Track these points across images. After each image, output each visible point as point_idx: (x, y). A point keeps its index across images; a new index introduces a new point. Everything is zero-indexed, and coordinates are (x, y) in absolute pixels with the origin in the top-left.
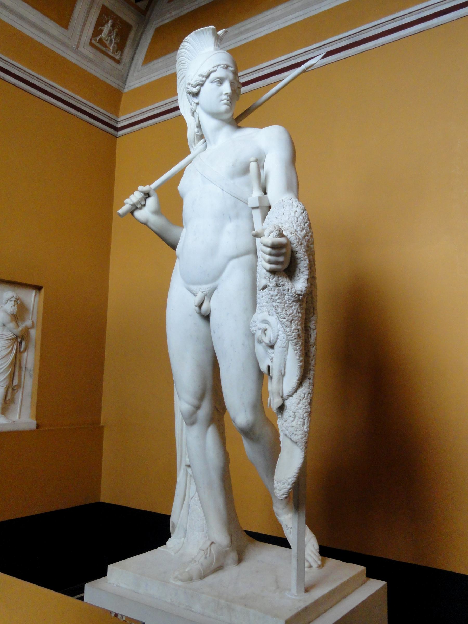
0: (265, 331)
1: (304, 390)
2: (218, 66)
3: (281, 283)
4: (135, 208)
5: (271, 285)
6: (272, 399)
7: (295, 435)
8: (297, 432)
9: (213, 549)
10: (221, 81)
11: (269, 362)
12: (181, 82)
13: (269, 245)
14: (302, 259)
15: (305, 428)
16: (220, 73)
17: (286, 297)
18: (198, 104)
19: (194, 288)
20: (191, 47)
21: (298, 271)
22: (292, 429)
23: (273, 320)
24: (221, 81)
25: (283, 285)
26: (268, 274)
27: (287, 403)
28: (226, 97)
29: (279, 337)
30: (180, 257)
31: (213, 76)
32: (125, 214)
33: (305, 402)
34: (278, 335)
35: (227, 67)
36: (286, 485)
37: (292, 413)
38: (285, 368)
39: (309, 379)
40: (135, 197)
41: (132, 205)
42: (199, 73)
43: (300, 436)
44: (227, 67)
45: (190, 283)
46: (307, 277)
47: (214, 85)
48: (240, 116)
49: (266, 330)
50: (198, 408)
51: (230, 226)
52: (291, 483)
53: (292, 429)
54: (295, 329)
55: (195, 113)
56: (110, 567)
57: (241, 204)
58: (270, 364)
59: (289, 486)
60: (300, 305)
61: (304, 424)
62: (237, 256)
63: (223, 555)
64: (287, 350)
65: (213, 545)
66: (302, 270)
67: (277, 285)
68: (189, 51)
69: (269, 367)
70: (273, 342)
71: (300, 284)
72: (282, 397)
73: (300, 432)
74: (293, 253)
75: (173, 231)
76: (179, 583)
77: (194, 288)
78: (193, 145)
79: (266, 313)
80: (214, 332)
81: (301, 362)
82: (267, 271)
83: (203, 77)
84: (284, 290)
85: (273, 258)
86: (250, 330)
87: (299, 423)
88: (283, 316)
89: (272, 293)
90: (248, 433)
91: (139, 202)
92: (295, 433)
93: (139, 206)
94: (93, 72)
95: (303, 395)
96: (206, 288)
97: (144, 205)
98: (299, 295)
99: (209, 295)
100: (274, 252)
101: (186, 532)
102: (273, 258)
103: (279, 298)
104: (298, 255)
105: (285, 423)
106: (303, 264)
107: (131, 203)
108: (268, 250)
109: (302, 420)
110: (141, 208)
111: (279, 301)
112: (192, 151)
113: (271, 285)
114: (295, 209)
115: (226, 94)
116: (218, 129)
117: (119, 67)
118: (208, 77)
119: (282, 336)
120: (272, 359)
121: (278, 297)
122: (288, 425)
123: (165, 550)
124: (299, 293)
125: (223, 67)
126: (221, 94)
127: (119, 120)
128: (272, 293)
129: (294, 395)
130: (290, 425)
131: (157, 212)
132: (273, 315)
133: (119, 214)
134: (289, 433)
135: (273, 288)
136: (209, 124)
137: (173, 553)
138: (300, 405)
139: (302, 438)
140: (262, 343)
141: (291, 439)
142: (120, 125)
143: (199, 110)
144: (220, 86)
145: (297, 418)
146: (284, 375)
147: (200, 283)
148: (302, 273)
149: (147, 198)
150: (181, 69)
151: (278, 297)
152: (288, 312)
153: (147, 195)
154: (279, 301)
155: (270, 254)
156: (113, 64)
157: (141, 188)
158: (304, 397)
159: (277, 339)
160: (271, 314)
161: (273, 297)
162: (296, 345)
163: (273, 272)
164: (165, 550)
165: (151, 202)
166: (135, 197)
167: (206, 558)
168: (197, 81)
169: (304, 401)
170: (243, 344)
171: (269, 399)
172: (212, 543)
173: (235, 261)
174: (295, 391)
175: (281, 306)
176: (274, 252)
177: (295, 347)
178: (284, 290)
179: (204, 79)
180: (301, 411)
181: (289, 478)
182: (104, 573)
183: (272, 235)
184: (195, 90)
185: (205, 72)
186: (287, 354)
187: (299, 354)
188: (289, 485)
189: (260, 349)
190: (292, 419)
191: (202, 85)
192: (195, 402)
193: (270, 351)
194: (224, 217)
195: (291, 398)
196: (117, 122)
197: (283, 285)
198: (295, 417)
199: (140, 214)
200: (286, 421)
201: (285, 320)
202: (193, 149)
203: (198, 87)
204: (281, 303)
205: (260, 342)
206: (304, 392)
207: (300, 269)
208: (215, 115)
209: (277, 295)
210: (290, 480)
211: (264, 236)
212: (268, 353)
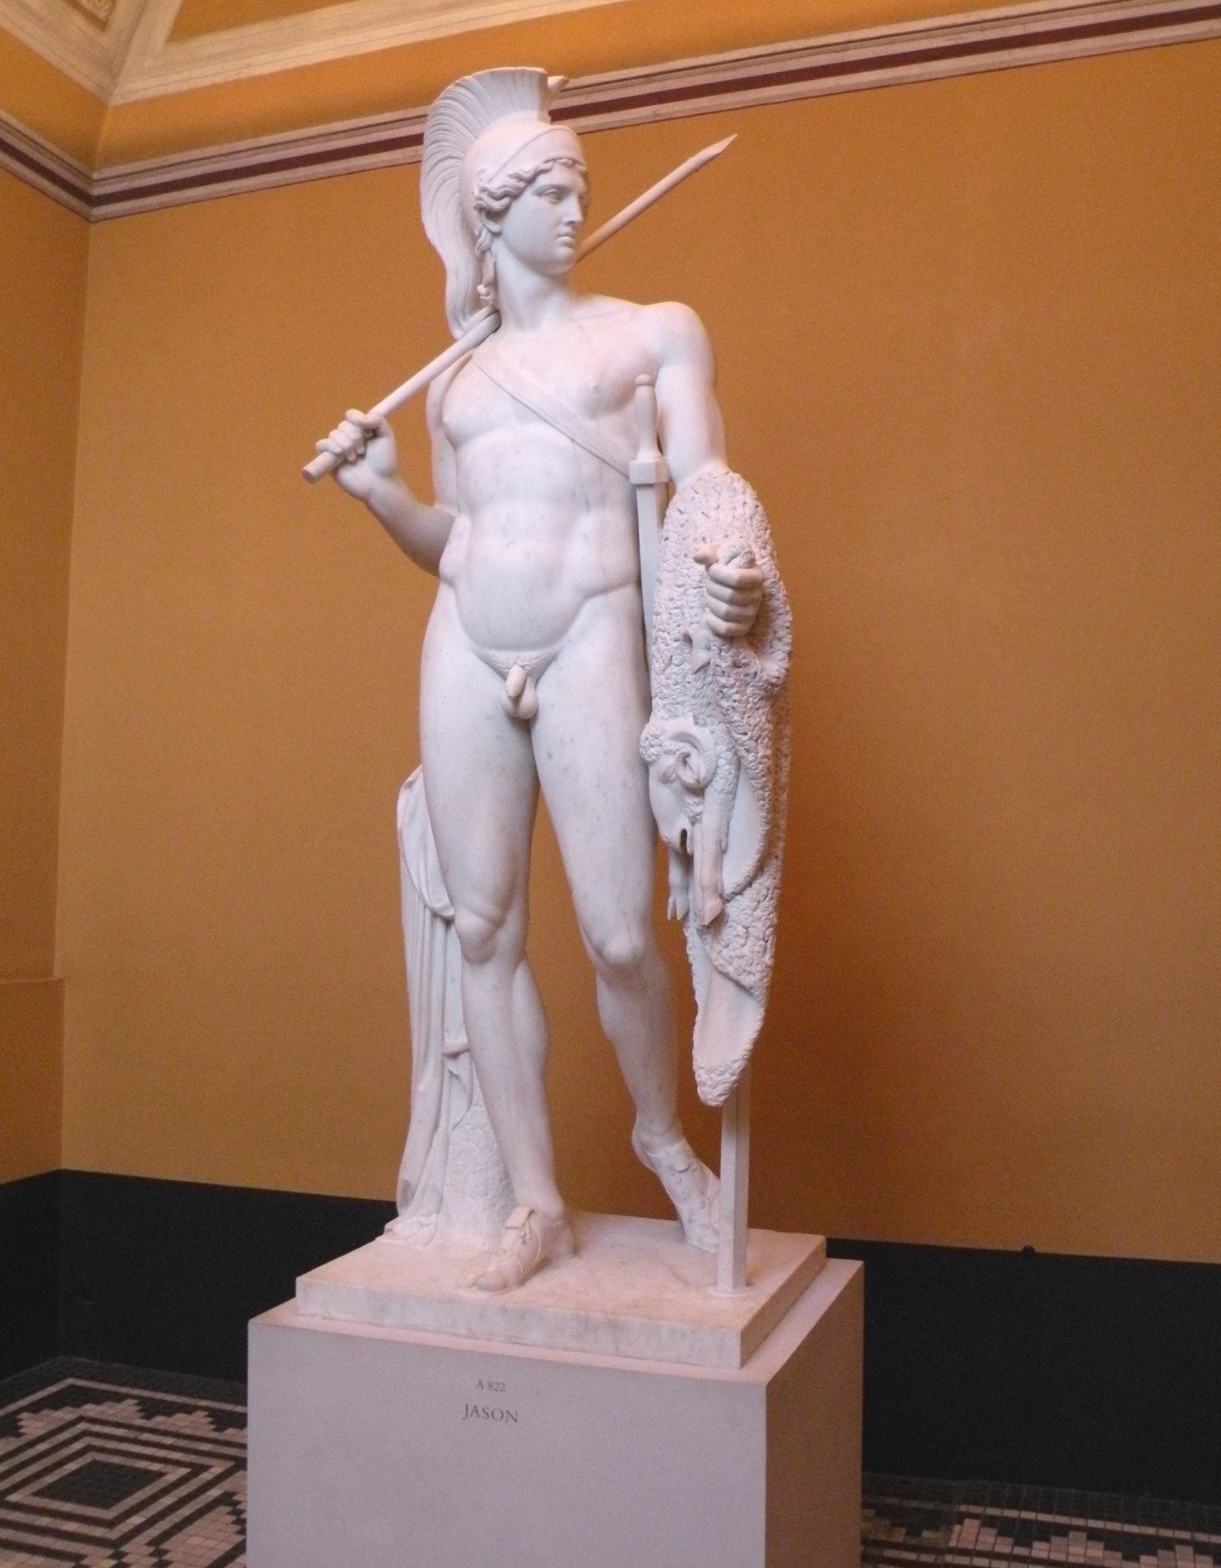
0: (685, 759)
1: (766, 882)
2: (554, 160)
3: (744, 661)
4: (343, 460)
5: (723, 665)
6: (679, 900)
7: (749, 973)
8: (752, 969)
9: (536, 1226)
10: (559, 193)
11: (683, 823)
12: (432, 169)
13: (734, 583)
14: (781, 611)
15: (768, 959)
16: (559, 176)
17: (749, 690)
18: (496, 235)
19: (501, 657)
20: (472, 97)
21: (770, 637)
22: (742, 962)
23: (710, 736)
24: (559, 193)
25: (746, 665)
26: (717, 642)
27: (733, 909)
28: (568, 229)
29: (719, 771)
30: (461, 583)
31: (543, 181)
32: (321, 475)
33: (768, 904)
34: (717, 767)
35: (572, 164)
36: (727, 1075)
37: (741, 930)
38: (727, 836)
39: (776, 857)
40: (343, 436)
41: (337, 455)
42: (512, 170)
43: (758, 976)
44: (572, 164)
45: (488, 645)
46: (788, 648)
47: (543, 202)
48: (588, 271)
49: (688, 755)
50: (497, 924)
51: (588, 522)
52: (738, 1071)
53: (742, 962)
54: (764, 757)
55: (488, 254)
56: (302, 1281)
57: (611, 475)
58: (688, 827)
59: (734, 1078)
60: (772, 706)
61: (765, 950)
62: (604, 590)
63: (551, 1236)
64: (734, 798)
65: (533, 1217)
66: (781, 633)
67: (736, 665)
68: (463, 104)
69: (684, 834)
70: (703, 782)
71: (773, 665)
72: (721, 896)
73: (759, 968)
74: (767, 596)
75: (424, 519)
76: (483, 1296)
77: (501, 657)
78: (460, 318)
79: (691, 720)
80: (550, 756)
81: (768, 823)
82: (717, 634)
83: (519, 178)
84: (746, 675)
85: (735, 610)
86: (638, 754)
87: (757, 949)
88: (742, 730)
89: (723, 680)
90: (625, 975)
91: (354, 448)
92: (748, 969)
93: (352, 458)
94: (38, 48)
95: (764, 892)
96: (531, 657)
97: (362, 456)
98: (772, 685)
99: (535, 674)
100: (738, 596)
101: (441, 1200)
102: (735, 610)
103: (737, 692)
104: (775, 603)
105: (725, 951)
106: (783, 621)
107: (338, 450)
108: (728, 592)
109: (763, 943)
110: (354, 463)
111: (736, 697)
112: (457, 333)
113: (723, 665)
114: (741, 498)
115: (571, 223)
116: (539, 297)
117: (104, 40)
118: (531, 181)
119: (726, 767)
120: (694, 820)
121: (735, 690)
122: (733, 954)
123: (394, 1242)
124: (774, 681)
125: (565, 164)
126: (558, 222)
127: (95, 176)
128: (723, 680)
129: (747, 892)
130: (738, 952)
131: (388, 474)
132: (705, 725)
133: (307, 476)
134: (736, 969)
135: (728, 670)
136: (519, 282)
137: (420, 1247)
138: (758, 913)
139: (761, 980)
140: (672, 782)
141: (738, 984)
142: (97, 191)
143: (498, 247)
144: (556, 203)
145: (751, 939)
146: (724, 852)
147: (518, 646)
148: (780, 639)
149: (371, 439)
150: (437, 141)
151: (735, 690)
152: (752, 721)
153: (371, 433)
154: (736, 697)
155: (730, 602)
156: (91, 30)
157: (355, 414)
158: (766, 896)
159: (714, 774)
160: (701, 721)
161: (725, 690)
162: (762, 788)
163: (729, 639)
164: (394, 1242)
165: (381, 450)
166: (343, 436)
167: (524, 1242)
168: (505, 186)
169: (766, 903)
170: (625, 784)
171: (671, 900)
172: (532, 1212)
173: (598, 601)
174: (749, 884)
175: (741, 708)
176: (738, 596)
177: (761, 792)
178: (746, 675)
179: (522, 184)
180: (760, 925)
181: (736, 1061)
182: (290, 1293)
183: (736, 561)
184: (497, 205)
185: (527, 168)
186: (733, 806)
187: (767, 806)
188: (733, 1074)
189: (663, 797)
190: (743, 941)
191: (514, 195)
192: (491, 909)
193: (691, 800)
194: (575, 499)
195: (739, 897)
196: (91, 181)
197: (746, 665)
198: (747, 938)
199: (359, 476)
200: (727, 946)
201: (745, 738)
202: (460, 325)
203: (505, 201)
204: (740, 701)
205: (665, 780)
206: (767, 884)
207: (775, 632)
208: (535, 263)
209: (733, 686)
210: (737, 1064)
211: (717, 561)
212: (686, 805)
